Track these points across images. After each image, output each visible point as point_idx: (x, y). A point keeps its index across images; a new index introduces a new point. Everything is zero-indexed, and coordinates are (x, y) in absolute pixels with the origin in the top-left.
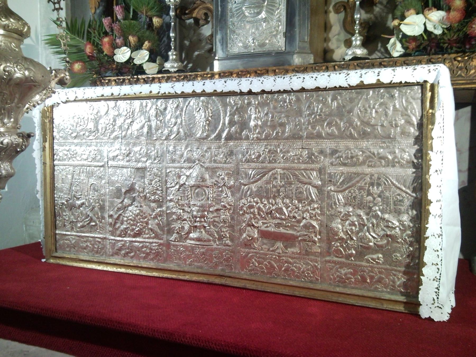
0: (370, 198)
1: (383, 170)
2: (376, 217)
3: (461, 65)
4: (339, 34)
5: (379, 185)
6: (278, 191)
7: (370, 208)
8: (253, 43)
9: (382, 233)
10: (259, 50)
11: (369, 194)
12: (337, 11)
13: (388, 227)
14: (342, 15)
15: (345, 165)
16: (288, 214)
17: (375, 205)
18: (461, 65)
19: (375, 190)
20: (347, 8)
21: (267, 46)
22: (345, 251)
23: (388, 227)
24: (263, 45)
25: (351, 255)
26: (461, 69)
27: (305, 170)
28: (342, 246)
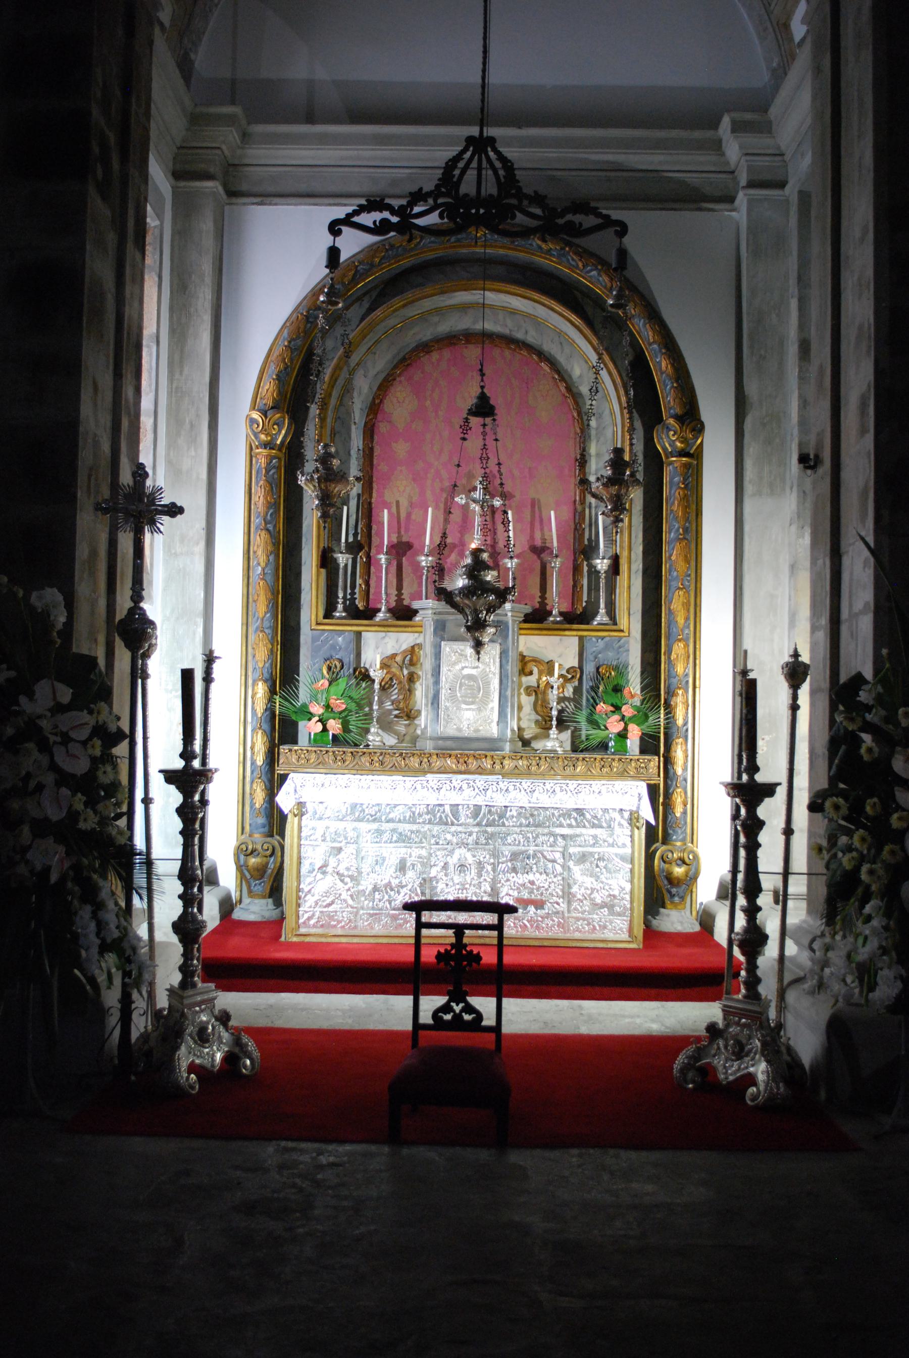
0: (598, 869)
1: (605, 849)
2: (602, 882)
3: (642, 765)
4: (530, 714)
5: (604, 860)
6: (531, 868)
7: (598, 877)
8: (468, 728)
9: (607, 893)
10: (474, 735)
11: (597, 866)
12: (529, 695)
13: (610, 888)
14: (533, 698)
15: (580, 846)
16: (251, 831)
17: (602, 874)
18: (642, 765)
19: (601, 864)
20: (538, 692)
21: (482, 732)
22: (581, 907)
23: (610, 888)
24: (477, 731)
25: (585, 911)
26: (643, 768)
27: (551, 851)
28: (579, 905)
